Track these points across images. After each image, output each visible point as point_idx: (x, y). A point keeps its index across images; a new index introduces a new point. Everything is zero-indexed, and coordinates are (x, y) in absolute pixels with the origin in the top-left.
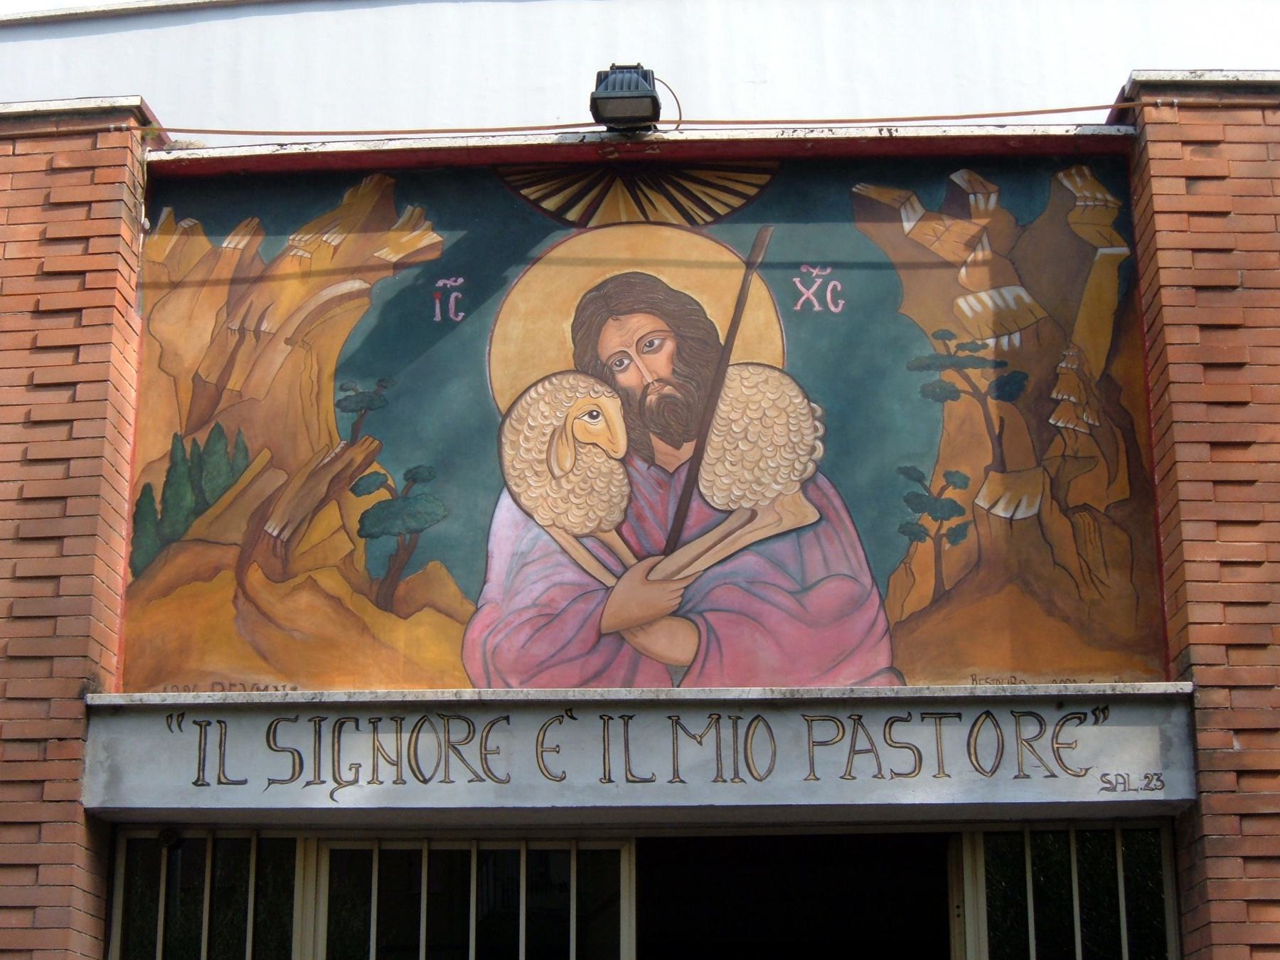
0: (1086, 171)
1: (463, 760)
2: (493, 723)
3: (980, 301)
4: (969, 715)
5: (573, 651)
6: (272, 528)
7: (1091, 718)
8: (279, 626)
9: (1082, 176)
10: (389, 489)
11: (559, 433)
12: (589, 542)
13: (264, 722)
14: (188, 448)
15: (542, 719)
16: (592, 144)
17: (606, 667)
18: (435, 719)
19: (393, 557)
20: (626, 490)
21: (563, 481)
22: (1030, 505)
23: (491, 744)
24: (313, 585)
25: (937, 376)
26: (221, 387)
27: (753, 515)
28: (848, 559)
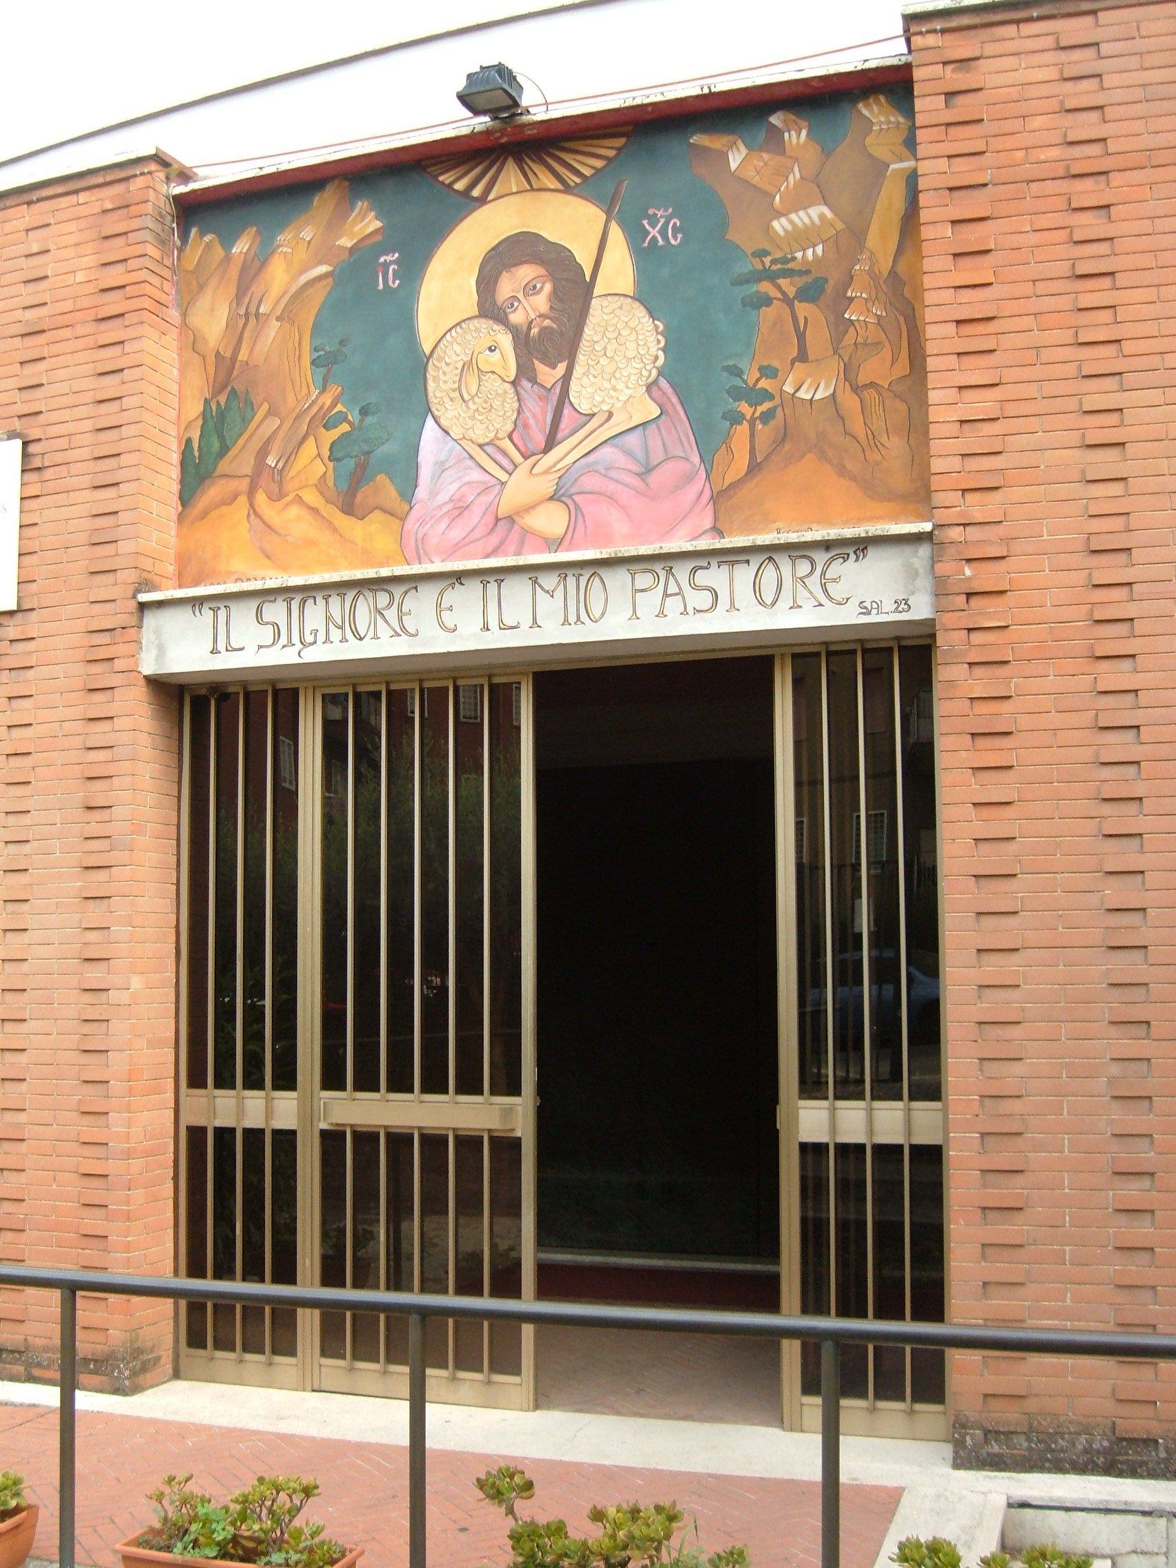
0: (882, 98)
1: (386, 621)
2: (406, 593)
3: (791, 222)
4: (755, 561)
5: (477, 534)
6: (271, 461)
7: (853, 557)
8: (277, 533)
9: (878, 103)
10: (349, 423)
11: (467, 365)
12: (489, 449)
13: (253, 604)
14: (214, 408)
15: (441, 585)
16: (480, 133)
17: (501, 543)
18: (367, 593)
19: (352, 475)
20: (516, 405)
21: (470, 403)
22: (827, 387)
23: (405, 609)
24: (299, 500)
25: (754, 288)
26: (234, 359)
27: (611, 415)
28: (682, 445)
